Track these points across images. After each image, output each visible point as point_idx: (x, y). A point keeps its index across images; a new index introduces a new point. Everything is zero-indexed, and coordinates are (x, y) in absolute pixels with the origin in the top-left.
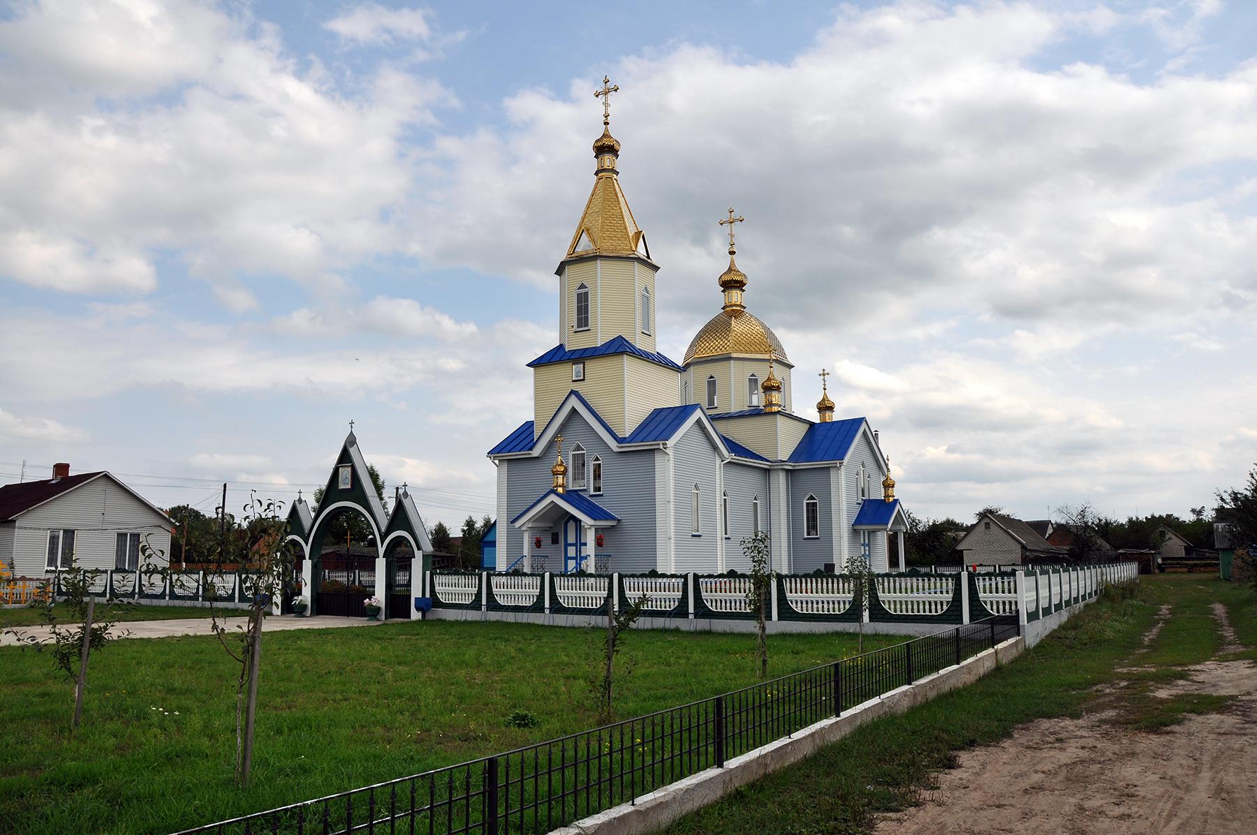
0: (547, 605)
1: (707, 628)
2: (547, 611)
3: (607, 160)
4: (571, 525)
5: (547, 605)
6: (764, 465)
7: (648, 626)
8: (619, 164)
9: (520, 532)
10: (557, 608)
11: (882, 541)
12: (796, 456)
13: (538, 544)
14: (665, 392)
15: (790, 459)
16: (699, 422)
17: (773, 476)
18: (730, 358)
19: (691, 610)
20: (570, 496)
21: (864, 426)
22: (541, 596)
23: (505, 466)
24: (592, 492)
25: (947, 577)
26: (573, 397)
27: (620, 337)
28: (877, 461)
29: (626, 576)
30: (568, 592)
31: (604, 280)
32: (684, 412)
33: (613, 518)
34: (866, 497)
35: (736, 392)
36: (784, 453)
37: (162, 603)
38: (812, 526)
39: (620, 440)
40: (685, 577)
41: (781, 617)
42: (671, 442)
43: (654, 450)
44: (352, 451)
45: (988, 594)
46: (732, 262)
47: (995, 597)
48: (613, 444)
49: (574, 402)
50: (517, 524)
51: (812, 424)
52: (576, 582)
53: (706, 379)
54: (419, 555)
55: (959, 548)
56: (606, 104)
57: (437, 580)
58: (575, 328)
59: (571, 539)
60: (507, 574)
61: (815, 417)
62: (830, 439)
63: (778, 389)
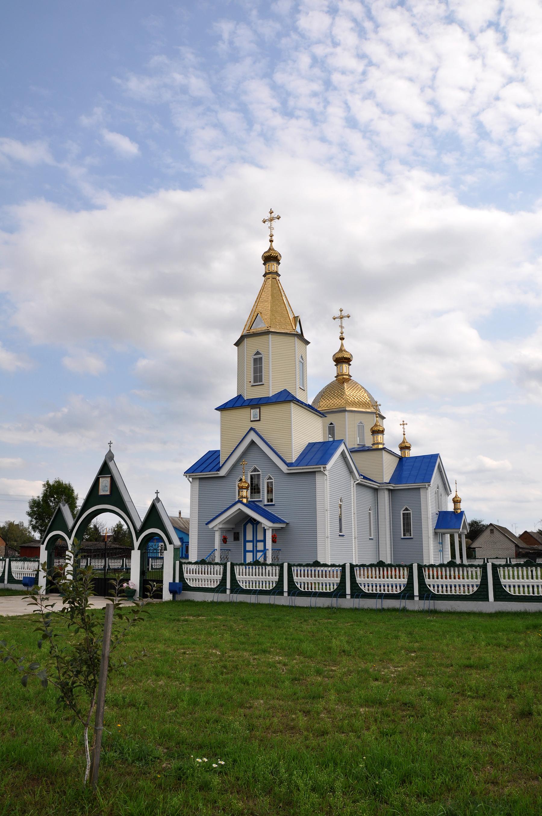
0: (286, 588)
1: (432, 608)
3: (273, 267)
4: (249, 528)
5: (286, 588)
7: (379, 606)
8: (281, 269)
9: (213, 531)
10: (294, 591)
13: (224, 540)
17: (380, 494)
18: (345, 411)
19: (416, 593)
20: (251, 505)
23: (197, 483)
24: (266, 503)
25: (476, 567)
26: (252, 433)
27: (285, 390)
28: (444, 484)
29: (237, 564)
30: (246, 578)
31: (274, 349)
35: (351, 433)
36: (387, 478)
37: (409, 605)
38: (407, 529)
39: (289, 465)
40: (343, 566)
43: (315, 472)
44: (111, 464)
45: (507, 580)
46: (342, 345)
47: (511, 581)
49: (252, 436)
50: (211, 526)
52: (250, 569)
53: (328, 425)
54: (170, 548)
56: (271, 228)
57: (13, 564)
58: (252, 383)
59: (249, 537)
60: (196, 563)
62: (416, 470)
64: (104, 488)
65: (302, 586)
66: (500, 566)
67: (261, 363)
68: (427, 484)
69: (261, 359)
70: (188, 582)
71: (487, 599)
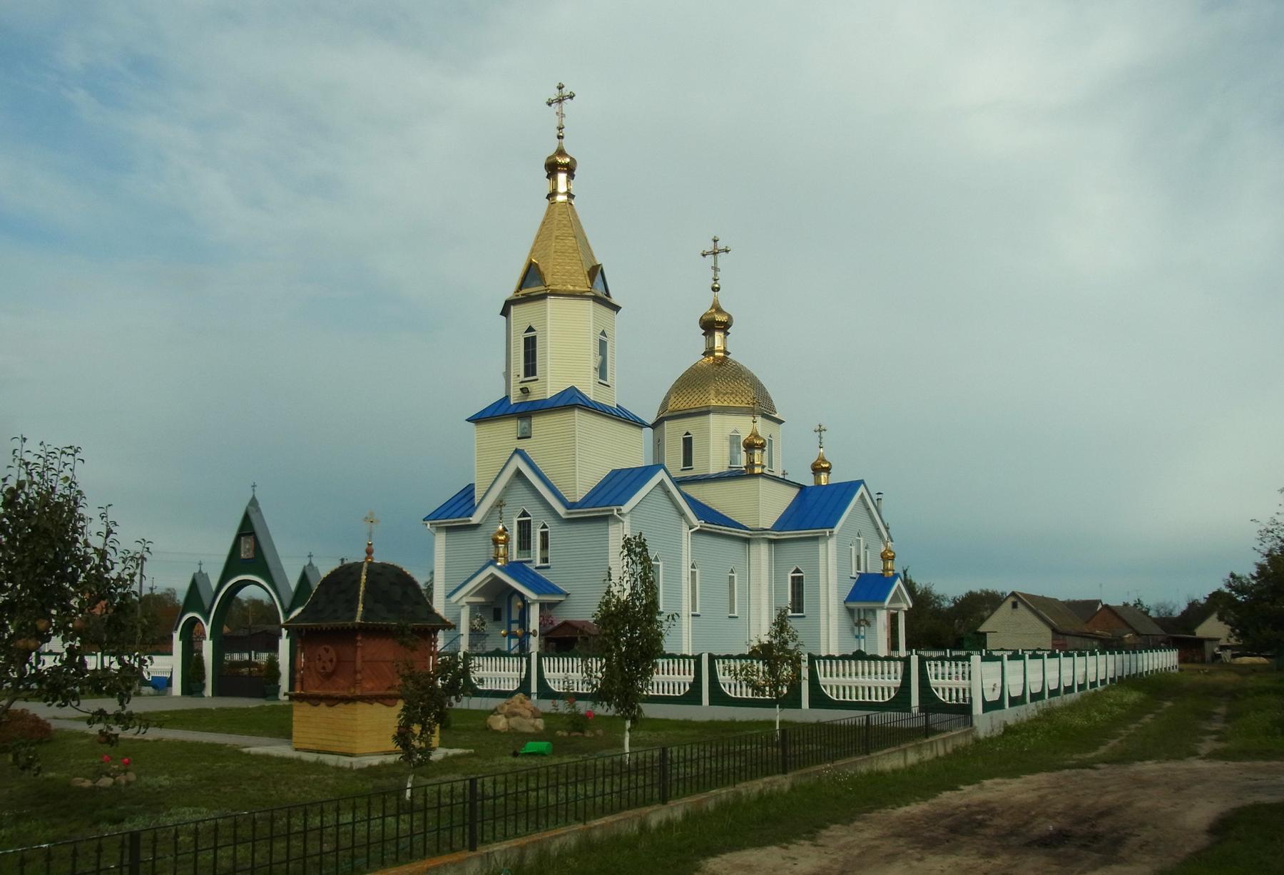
2: (534, 697)
6: (743, 533)
11: (882, 618)
12: (781, 524)
14: (632, 449)
15: (775, 528)
16: (662, 484)
21: (862, 489)
22: (697, 684)
24: (538, 564)
27: (573, 388)
32: (644, 474)
33: (561, 593)
34: (862, 571)
39: (570, 506)
40: (698, 659)
41: (712, 702)
42: (626, 508)
47: (946, 683)
48: (561, 510)
49: (518, 463)
50: (454, 599)
51: (802, 488)
55: (981, 629)
61: (809, 481)
63: (762, 447)
64: (246, 552)
65: (947, 695)
66: (931, 659)
67: (534, 345)
68: (827, 531)
69: (534, 338)
70: (551, 685)
71: (699, 702)
